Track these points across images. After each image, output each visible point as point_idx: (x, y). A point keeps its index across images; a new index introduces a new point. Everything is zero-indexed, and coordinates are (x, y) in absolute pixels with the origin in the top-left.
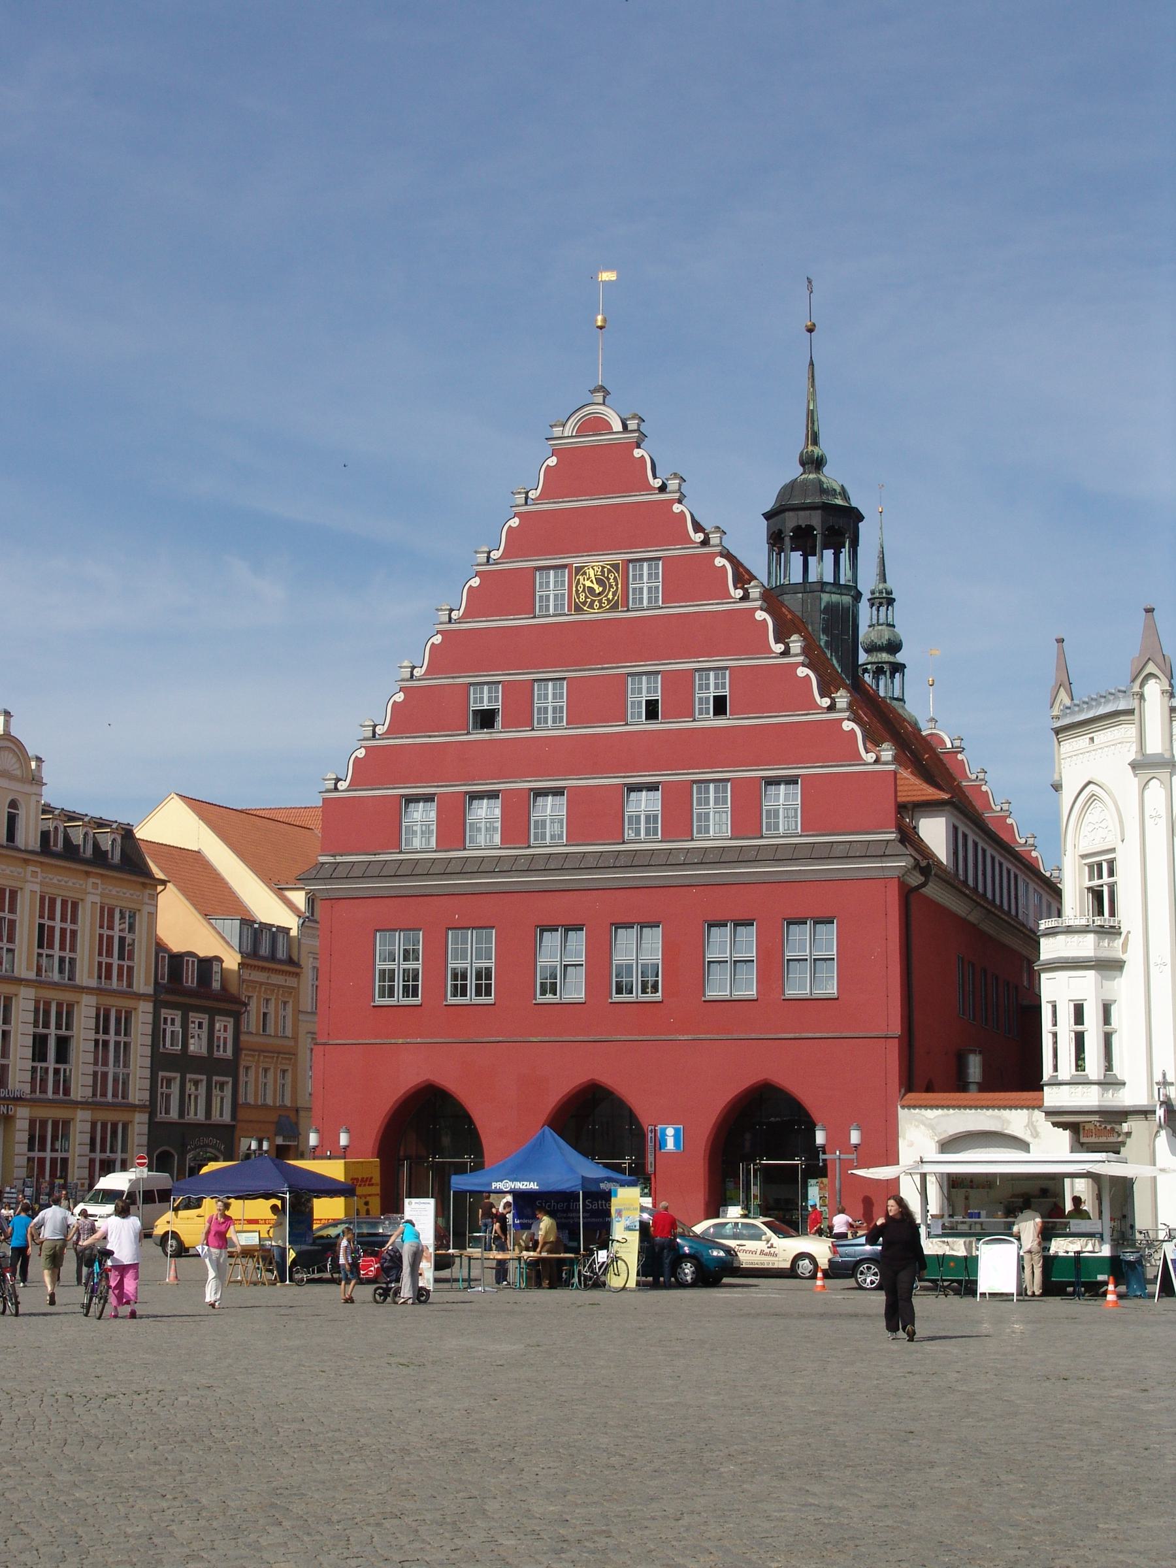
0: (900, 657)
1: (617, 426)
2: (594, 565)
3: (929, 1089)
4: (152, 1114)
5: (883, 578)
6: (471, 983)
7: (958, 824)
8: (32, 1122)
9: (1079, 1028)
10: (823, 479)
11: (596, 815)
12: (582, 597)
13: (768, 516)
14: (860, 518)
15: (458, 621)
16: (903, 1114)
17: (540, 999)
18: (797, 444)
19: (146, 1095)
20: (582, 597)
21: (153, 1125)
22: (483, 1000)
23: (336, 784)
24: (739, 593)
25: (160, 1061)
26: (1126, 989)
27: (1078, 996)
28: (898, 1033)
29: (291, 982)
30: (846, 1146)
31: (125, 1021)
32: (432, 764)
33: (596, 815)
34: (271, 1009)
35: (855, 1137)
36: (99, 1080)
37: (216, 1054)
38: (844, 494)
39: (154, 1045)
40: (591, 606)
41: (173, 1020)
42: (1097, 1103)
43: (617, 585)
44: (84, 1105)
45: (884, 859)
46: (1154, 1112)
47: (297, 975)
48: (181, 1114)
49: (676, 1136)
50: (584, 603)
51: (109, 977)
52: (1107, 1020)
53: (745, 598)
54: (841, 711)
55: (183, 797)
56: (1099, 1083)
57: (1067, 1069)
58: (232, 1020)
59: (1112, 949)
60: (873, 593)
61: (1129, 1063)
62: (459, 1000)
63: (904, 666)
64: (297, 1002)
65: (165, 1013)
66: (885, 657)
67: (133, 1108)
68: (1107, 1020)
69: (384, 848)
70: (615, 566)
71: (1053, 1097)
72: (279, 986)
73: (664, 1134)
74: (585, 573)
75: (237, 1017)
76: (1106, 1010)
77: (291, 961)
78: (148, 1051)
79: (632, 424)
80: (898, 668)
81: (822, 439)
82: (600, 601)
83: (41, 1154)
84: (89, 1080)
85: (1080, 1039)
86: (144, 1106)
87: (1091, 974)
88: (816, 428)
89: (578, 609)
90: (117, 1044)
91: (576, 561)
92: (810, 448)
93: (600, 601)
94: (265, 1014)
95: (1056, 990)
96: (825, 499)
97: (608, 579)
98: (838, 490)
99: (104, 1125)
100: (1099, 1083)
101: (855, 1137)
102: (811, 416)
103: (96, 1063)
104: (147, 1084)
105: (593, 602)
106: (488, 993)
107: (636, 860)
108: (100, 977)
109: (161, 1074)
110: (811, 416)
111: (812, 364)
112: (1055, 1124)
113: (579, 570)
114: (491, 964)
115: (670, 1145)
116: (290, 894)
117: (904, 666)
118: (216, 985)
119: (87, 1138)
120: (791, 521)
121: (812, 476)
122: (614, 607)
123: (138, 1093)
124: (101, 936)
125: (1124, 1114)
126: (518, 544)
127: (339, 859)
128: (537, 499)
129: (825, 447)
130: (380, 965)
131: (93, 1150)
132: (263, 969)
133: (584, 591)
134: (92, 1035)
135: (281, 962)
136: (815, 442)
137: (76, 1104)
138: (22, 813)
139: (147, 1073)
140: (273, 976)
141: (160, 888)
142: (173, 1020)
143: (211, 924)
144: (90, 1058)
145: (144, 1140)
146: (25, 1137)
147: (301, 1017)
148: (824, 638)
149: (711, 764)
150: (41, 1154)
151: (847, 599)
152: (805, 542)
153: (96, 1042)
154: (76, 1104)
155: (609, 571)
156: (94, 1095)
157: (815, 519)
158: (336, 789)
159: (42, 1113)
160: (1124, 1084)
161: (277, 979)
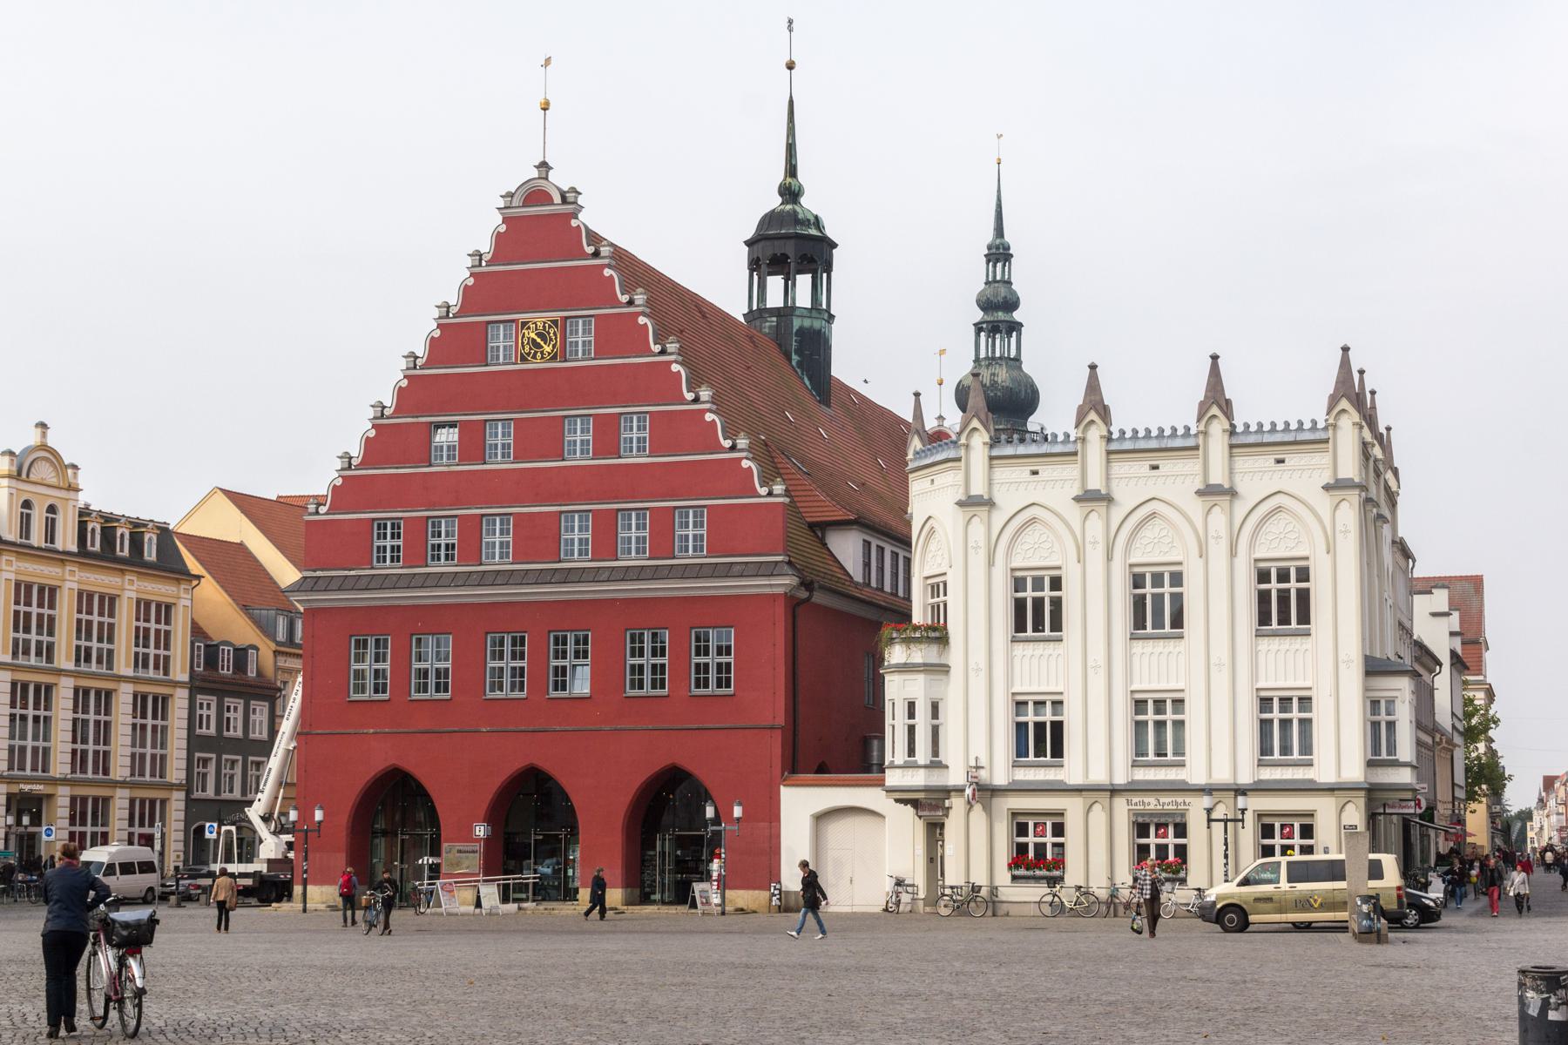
0: (1017, 316)
2: (540, 318)
3: (821, 770)
4: (189, 792)
7: (868, 538)
8: (73, 799)
9: (911, 722)
10: (798, 208)
11: (537, 539)
13: (749, 243)
16: (785, 792)
17: (490, 695)
19: (183, 775)
21: (189, 801)
22: (442, 696)
24: (657, 348)
25: (195, 742)
27: (911, 696)
28: (781, 720)
30: (731, 820)
31: (161, 705)
32: (397, 493)
33: (537, 539)
35: (737, 812)
36: (137, 762)
37: (252, 736)
39: (191, 728)
40: (534, 357)
42: (344, 855)
44: (123, 784)
46: (963, 791)
48: (218, 791)
51: (145, 666)
52: (935, 715)
54: (742, 450)
56: (925, 767)
57: (900, 756)
60: (989, 248)
61: (952, 752)
66: (1001, 315)
67: (171, 787)
68: (935, 715)
70: (555, 322)
71: (893, 778)
76: (935, 709)
78: (184, 734)
80: (1015, 327)
83: (82, 829)
84: (128, 761)
85: (911, 729)
86: (180, 785)
87: (921, 677)
89: (524, 359)
90: (154, 728)
92: (789, 180)
95: (897, 689)
99: (143, 802)
100: (925, 767)
101: (737, 812)
103: (133, 745)
104: (183, 764)
106: (446, 690)
107: (568, 576)
108: (136, 665)
109: (197, 755)
111: (791, 102)
112: (897, 801)
113: (524, 324)
114: (449, 665)
118: (252, 673)
119: (126, 814)
120: (768, 250)
121: (789, 207)
122: (554, 358)
123: (176, 771)
124: (137, 628)
125: (947, 792)
127: (319, 573)
131: (131, 824)
134: (130, 720)
137: (116, 784)
139: (184, 754)
141: (195, 583)
142: (209, 707)
144: (128, 740)
145: (182, 815)
146: (65, 812)
150: (82, 829)
153: (134, 726)
154: (116, 784)
156: (132, 775)
157: (789, 249)
158: (317, 513)
159: (81, 791)
160: (947, 767)
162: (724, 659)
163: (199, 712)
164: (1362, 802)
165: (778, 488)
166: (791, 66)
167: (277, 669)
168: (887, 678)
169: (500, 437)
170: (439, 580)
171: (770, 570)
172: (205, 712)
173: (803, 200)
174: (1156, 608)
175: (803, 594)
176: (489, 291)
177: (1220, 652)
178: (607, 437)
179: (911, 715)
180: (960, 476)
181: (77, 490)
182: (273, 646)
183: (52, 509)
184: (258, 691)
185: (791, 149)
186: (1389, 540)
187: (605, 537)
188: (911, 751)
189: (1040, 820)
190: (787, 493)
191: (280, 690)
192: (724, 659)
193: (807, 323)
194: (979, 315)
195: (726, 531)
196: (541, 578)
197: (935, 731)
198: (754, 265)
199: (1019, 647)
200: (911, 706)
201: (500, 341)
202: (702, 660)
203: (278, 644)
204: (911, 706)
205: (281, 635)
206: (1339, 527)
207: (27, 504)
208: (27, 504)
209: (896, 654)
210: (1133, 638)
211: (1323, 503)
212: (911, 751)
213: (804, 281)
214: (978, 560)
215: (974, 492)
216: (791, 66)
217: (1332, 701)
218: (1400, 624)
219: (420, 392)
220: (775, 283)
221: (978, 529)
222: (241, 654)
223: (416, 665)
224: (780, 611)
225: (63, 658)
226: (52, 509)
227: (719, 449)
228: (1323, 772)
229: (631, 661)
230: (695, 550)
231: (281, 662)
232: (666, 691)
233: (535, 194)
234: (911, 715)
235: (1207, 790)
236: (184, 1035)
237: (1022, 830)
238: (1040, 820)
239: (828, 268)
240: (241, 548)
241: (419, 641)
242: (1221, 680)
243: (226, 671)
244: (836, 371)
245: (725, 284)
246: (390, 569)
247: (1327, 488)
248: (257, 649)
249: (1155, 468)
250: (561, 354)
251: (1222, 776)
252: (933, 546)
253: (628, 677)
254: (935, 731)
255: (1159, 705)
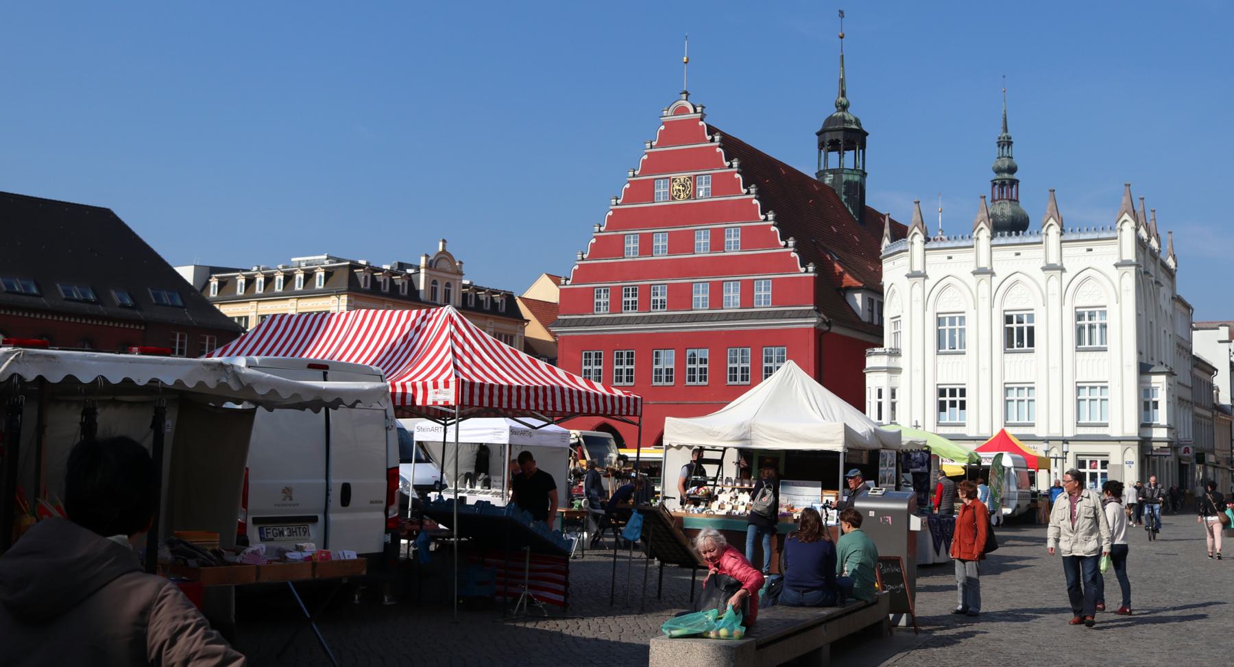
0: (1015, 176)
1: (692, 110)
2: (682, 176)
5: (1006, 130)
6: (664, 375)
11: (681, 297)
13: (818, 134)
14: (867, 134)
15: (622, 204)
18: (835, 96)
22: (703, 383)
26: (901, 381)
32: (607, 273)
38: (857, 122)
53: (748, 193)
55: (549, 276)
59: (895, 362)
62: (733, 383)
63: (1018, 181)
66: (1006, 176)
69: (586, 312)
79: (699, 109)
80: (1014, 182)
81: (847, 94)
85: (880, 405)
89: (673, 199)
91: (673, 176)
96: (846, 126)
102: (842, 81)
110: (842, 81)
114: (748, 365)
117: (1018, 181)
121: (840, 114)
122: (689, 198)
126: (648, 168)
130: (729, 365)
136: (843, 95)
138: (452, 289)
148: (844, 197)
151: (857, 178)
152: (834, 146)
157: (840, 136)
162: (703, 366)
164: (1136, 448)
165: (811, 269)
168: (868, 375)
169: (661, 241)
170: (628, 321)
171: (806, 315)
174: (1018, 335)
175: (826, 328)
177: (985, 362)
178: (717, 241)
179: (880, 396)
180: (1115, 248)
181: (462, 274)
183: (448, 285)
186: (1169, 296)
187: (716, 296)
188: (880, 418)
189: (1093, 458)
190: (815, 271)
192: (703, 366)
193: (850, 178)
194: (994, 176)
195: (781, 292)
196: (682, 319)
197: (893, 405)
198: (821, 145)
199: (1080, 354)
200: (880, 391)
201: (661, 190)
202: (630, 367)
204: (880, 391)
206: (1123, 288)
207: (435, 282)
208: (435, 282)
209: (871, 362)
210: (938, 353)
211: (1115, 273)
212: (880, 418)
213: (850, 154)
214: (918, 307)
215: (1125, 258)
217: (1119, 389)
218: (1179, 345)
220: (833, 156)
221: (918, 289)
223: (655, 367)
224: (812, 336)
226: (448, 285)
227: (778, 246)
228: (1114, 431)
229: (616, 367)
234: (880, 396)
235: (1047, 440)
237: (1082, 464)
238: (1093, 458)
239: (863, 147)
241: (657, 354)
242: (985, 378)
244: (867, 204)
245: (804, 159)
246: (631, 313)
247: (1117, 266)
249: (1018, 254)
250: (694, 195)
251: (1055, 432)
252: (894, 300)
254: (893, 405)
255: (953, 393)
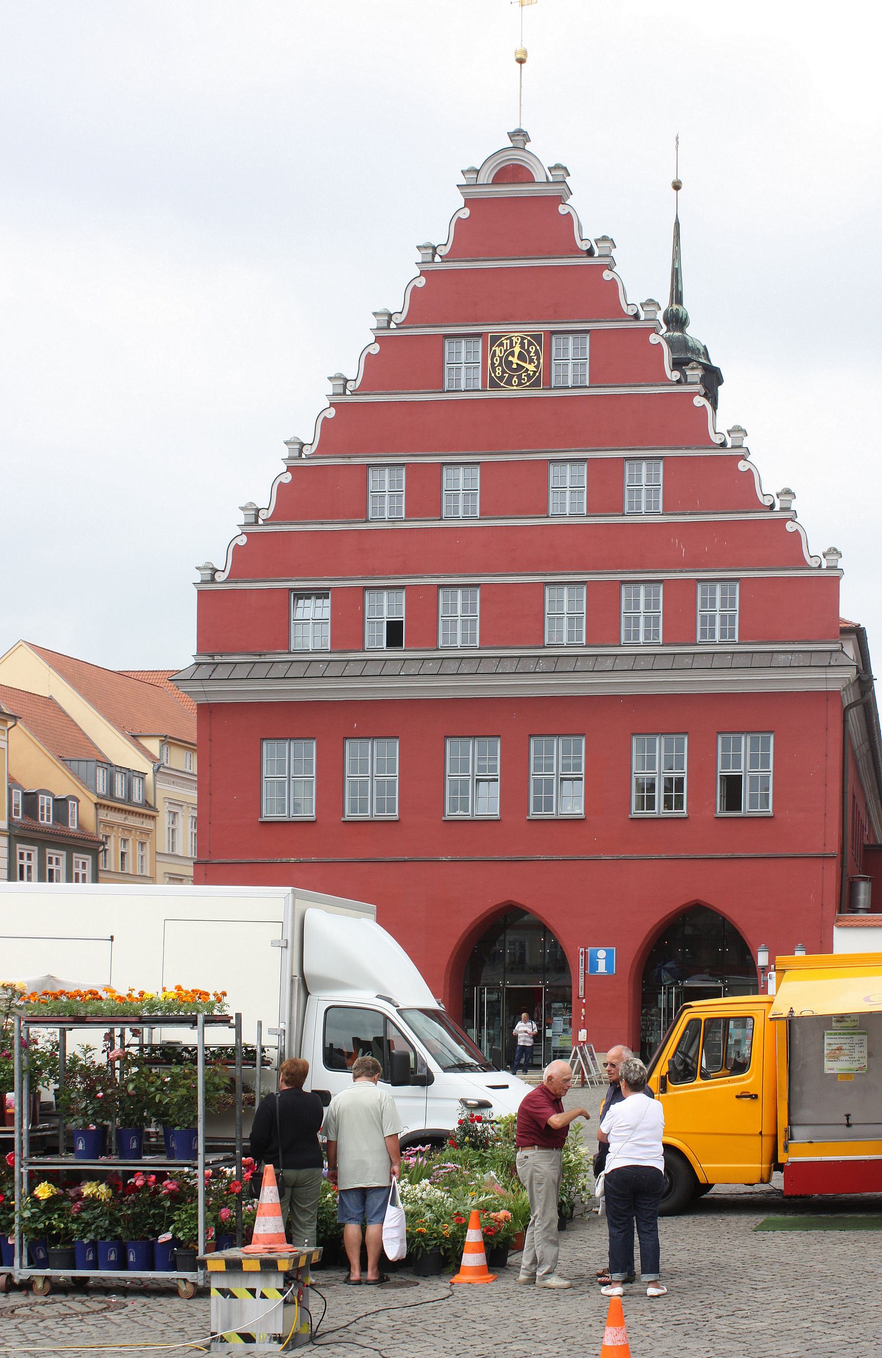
2: (516, 333)
12: (499, 371)
20: (499, 371)
23: (213, 576)
28: (834, 849)
29: (147, 824)
32: (324, 555)
34: (129, 849)
38: (706, 354)
40: (509, 382)
41: (29, 856)
43: (538, 359)
45: (829, 670)
47: (153, 818)
49: (608, 959)
50: (501, 378)
58: (90, 857)
64: (154, 844)
65: (20, 847)
70: (537, 338)
72: (137, 829)
73: (595, 959)
74: (501, 344)
75: (95, 853)
77: (146, 804)
82: (519, 377)
88: (680, 289)
89: (494, 385)
92: (675, 307)
93: (519, 377)
94: (123, 854)
97: (529, 352)
98: (702, 350)
105: (511, 377)
111: (677, 224)
113: (495, 339)
115: (602, 968)
116: (145, 742)
118: (73, 826)
122: (536, 384)
128: (446, 256)
129: (690, 306)
132: (120, 810)
133: (500, 364)
135: (137, 805)
140: (130, 818)
143: (69, 769)
147: (159, 858)
149: (642, 567)
155: (530, 344)
161: (132, 821)
163: (19, 862)
166: (677, 186)
167: (99, 822)
172: (25, 863)
173: (688, 330)
176: (447, 295)
178: (606, 488)
182: (95, 799)
184: (81, 843)
185: (676, 274)
187: (604, 618)
191: (104, 844)
203: (99, 796)
205: (102, 788)
216: (677, 186)
219: (353, 425)
222: (61, 804)
225: (15, 1300)
230: (723, 635)
231: (103, 814)
232: (684, 812)
233: (512, 172)
236: (45, 1332)
240: (50, 702)
243: (46, 821)
248: (78, 801)
253: (685, 794)
